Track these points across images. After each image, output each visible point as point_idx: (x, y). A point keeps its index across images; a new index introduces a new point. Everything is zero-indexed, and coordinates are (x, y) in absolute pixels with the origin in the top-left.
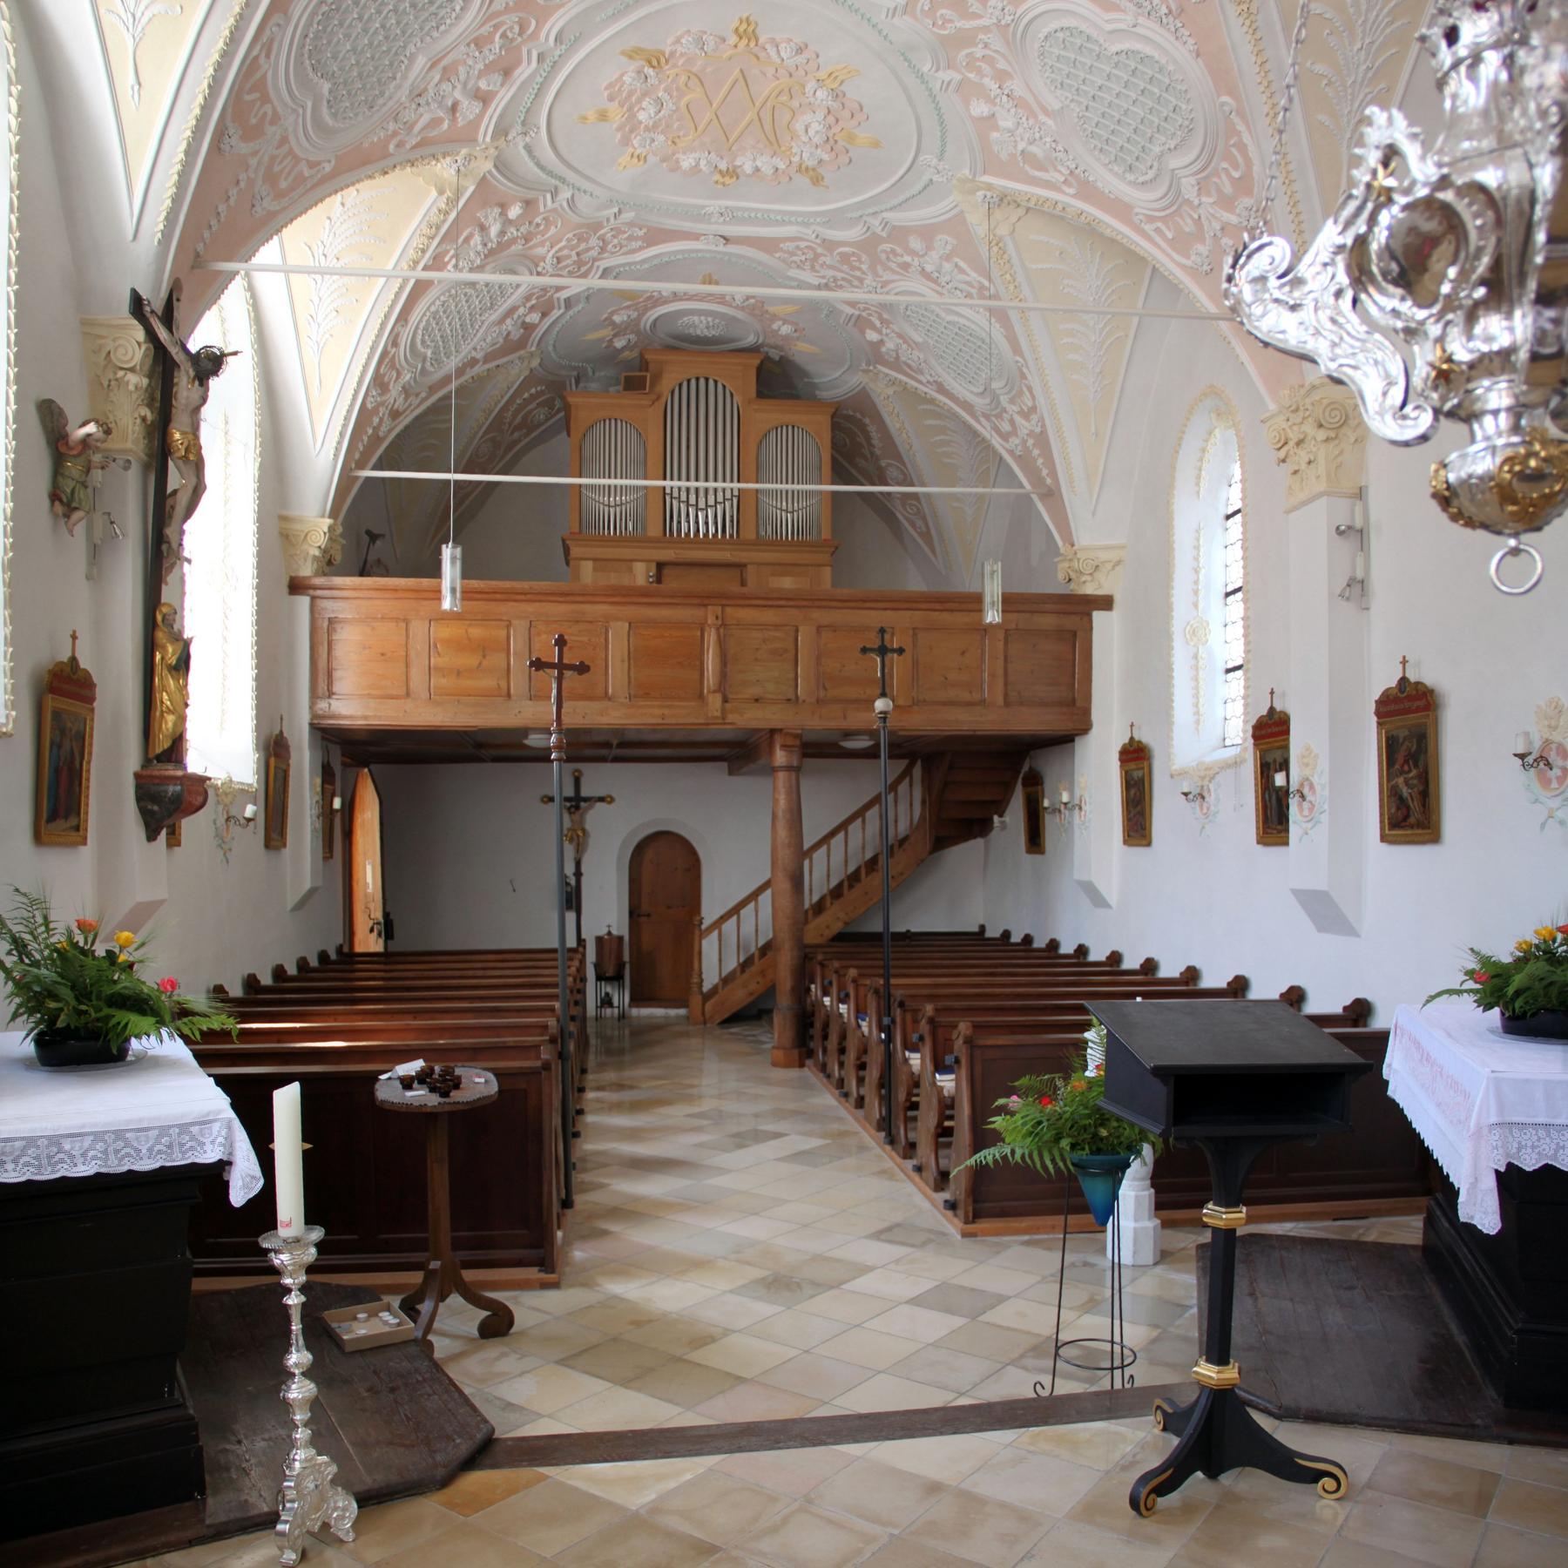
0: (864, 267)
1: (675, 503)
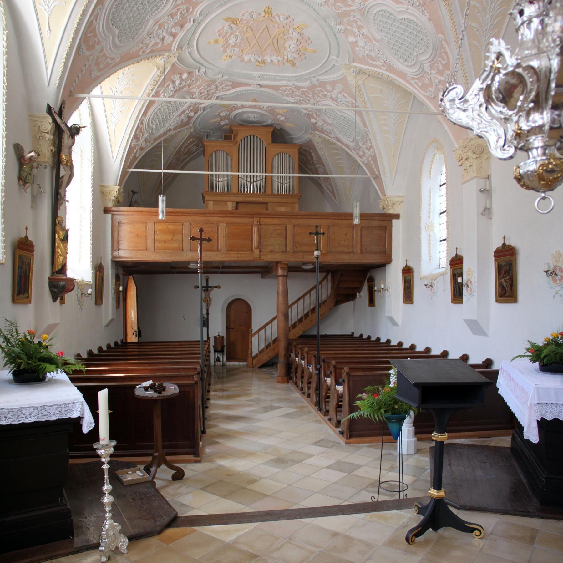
0: (310, 96)
1: (242, 181)
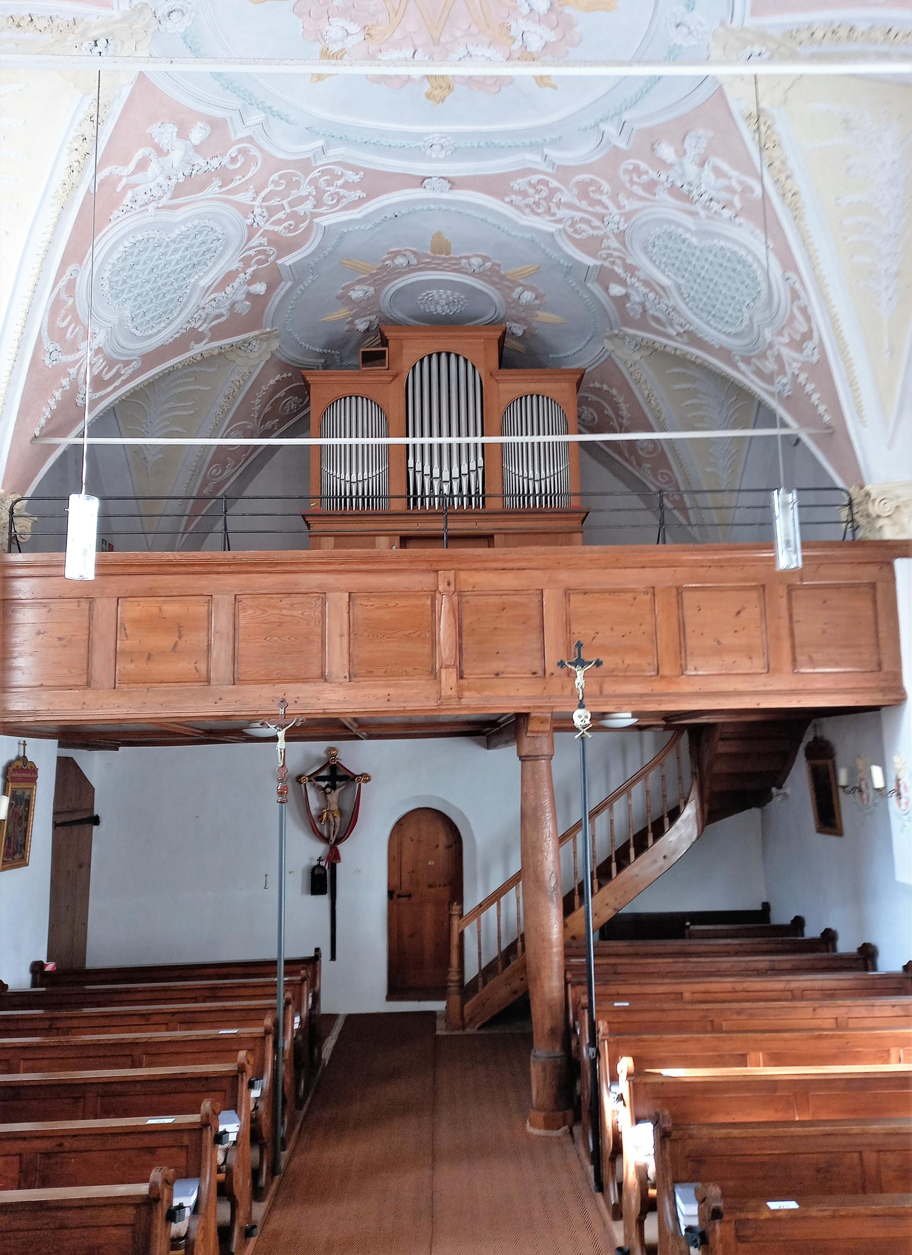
0: (605, 199)
1: (419, 476)
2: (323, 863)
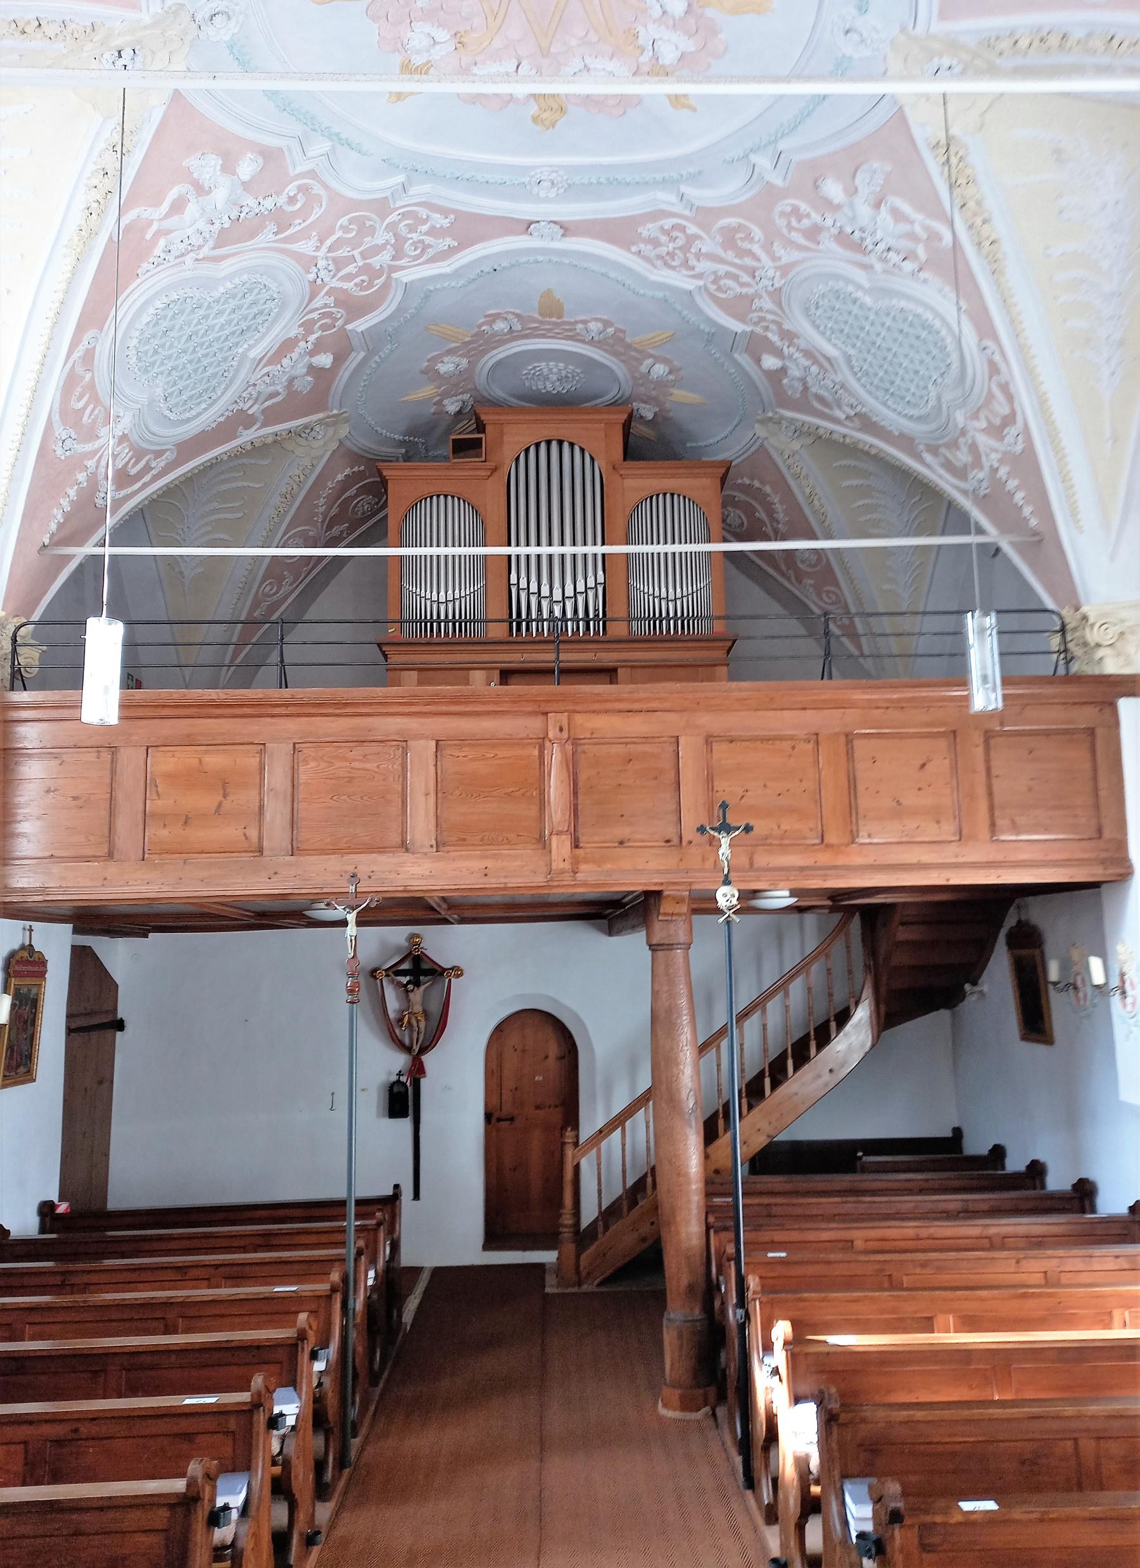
0: (756, 249)
1: (523, 595)
2: (403, 1079)
